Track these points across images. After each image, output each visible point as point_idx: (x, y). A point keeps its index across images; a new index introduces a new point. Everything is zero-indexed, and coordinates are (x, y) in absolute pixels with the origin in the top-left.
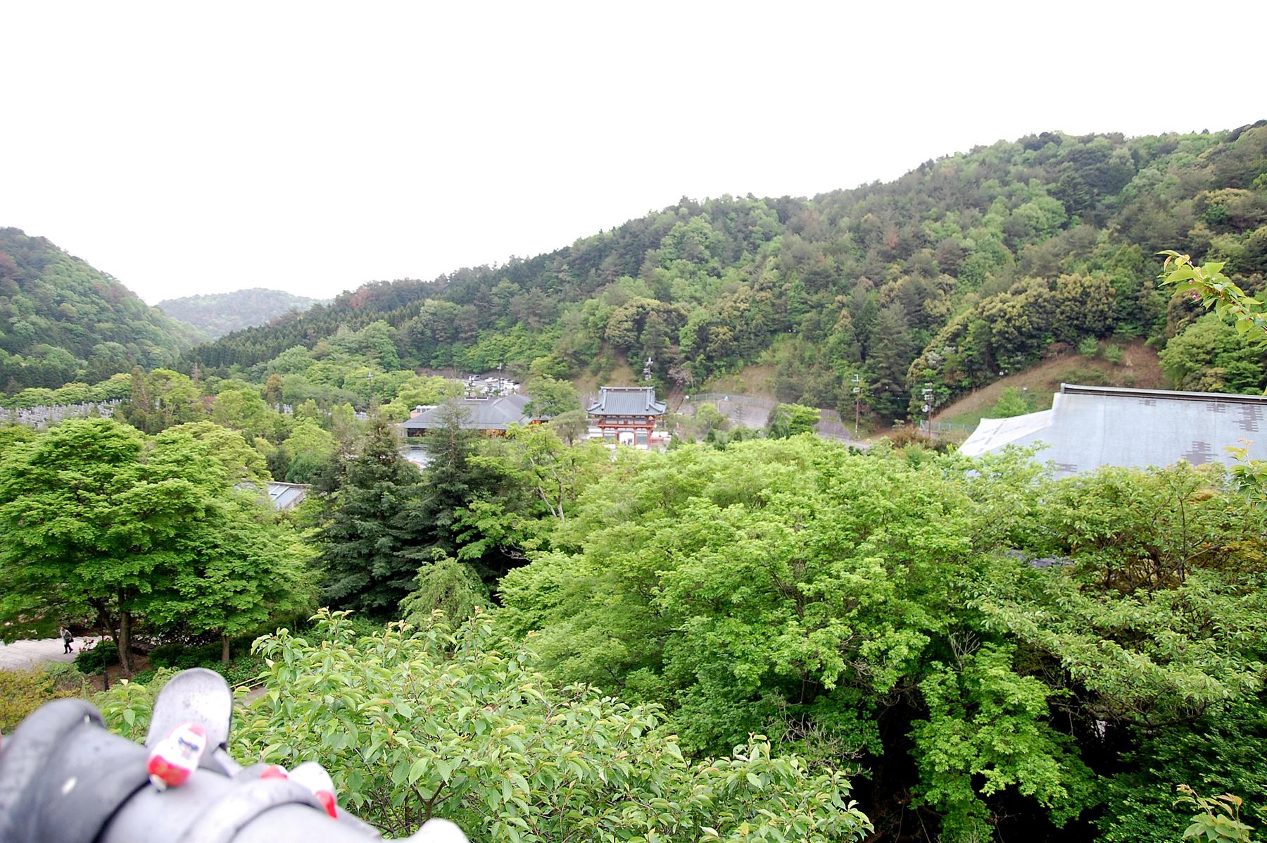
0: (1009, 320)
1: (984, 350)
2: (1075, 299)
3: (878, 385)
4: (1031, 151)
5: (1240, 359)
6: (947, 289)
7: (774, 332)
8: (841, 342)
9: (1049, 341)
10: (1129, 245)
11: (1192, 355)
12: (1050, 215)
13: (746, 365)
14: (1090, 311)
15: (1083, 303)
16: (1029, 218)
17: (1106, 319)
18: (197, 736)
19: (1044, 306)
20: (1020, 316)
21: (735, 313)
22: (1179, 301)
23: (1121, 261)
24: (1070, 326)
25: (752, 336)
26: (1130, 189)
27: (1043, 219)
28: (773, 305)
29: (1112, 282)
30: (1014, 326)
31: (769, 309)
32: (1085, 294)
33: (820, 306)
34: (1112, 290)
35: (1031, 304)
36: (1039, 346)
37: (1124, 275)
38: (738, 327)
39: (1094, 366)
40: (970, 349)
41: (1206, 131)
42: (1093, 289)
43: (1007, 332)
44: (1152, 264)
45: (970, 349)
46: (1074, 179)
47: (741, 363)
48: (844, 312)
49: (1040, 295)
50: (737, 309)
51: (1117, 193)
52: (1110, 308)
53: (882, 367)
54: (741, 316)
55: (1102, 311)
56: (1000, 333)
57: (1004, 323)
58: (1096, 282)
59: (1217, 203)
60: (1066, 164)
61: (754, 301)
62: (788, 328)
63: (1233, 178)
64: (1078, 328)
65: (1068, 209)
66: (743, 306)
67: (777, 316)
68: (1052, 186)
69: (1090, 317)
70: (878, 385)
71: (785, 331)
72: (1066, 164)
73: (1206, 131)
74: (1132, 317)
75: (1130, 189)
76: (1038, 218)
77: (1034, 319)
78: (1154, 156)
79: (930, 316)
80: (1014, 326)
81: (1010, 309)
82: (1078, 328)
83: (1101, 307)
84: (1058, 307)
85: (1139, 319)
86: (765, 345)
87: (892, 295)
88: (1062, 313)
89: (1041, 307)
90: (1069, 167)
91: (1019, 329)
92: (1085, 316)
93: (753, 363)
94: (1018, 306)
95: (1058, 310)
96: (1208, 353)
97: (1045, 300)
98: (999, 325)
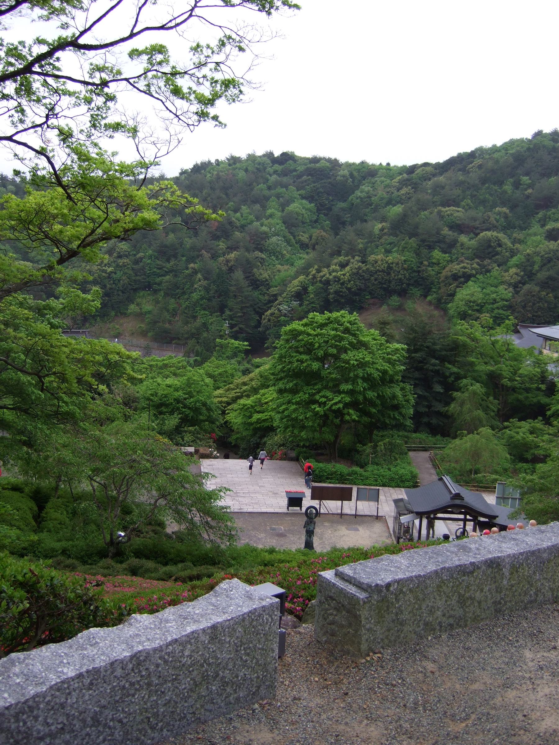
0: (343, 284)
1: (322, 303)
2: (383, 271)
3: (236, 329)
4: (277, 165)
5: (498, 308)
6: (262, 261)
7: (135, 290)
8: (202, 298)
9: (367, 297)
10: (410, 239)
11: (470, 307)
12: (309, 213)
13: (116, 315)
14: (393, 279)
15: (389, 274)
16: (297, 213)
17: (403, 284)
18: (289, 490)
19: (363, 276)
20: (350, 281)
21: (104, 274)
22: (450, 274)
23: (406, 248)
24: (381, 288)
25: (120, 293)
26: (354, 199)
27: (306, 215)
28: (133, 269)
29: (405, 261)
30: (346, 288)
31: (130, 272)
32: (390, 268)
33: (174, 272)
34: (405, 266)
35: (354, 274)
36: (360, 301)
37: (409, 256)
38: (108, 286)
39: (398, 314)
40: (313, 303)
41: (388, 164)
42: (394, 265)
43: (341, 292)
44: (425, 251)
45: (313, 303)
46: (318, 189)
47: (113, 313)
48: (199, 276)
49: (359, 268)
50: (105, 271)
51: (345, 201)
52: (405, 277)
53: (239, 316)
54: (109, 277)
55: (401, 279)
56: (336, 292)
57: (340, 286)
58: (396, 261)
59: (448, 215)
60: (305, 177)
61: (118, 266)
62: (148, 287)
63: (449, 200)
64: (385, 289)
65: (318, 210)
66: (110, 270)
67: (138, 278)
68: (302, 192)
69: (393, 283)
70: (236, 329)
71: (144, 289)
72: (305, 177)
73: (388, 164)
74: (417, 284)
75: (354, 199)
76: (303, 214)
77: (358, 283)
78: (364, 178)
79: (259, 280)
80: (346, 288)
81: (342, 276)
82: (385, 289)
83: (400, 276)
84: (371, 276)
85: (421, 285)
86: (131, 300)
87: (230, 265)
88: (376, 280)
89: (361, 276)
90: (309, 180)
91: (349, 289)
92: (390, 282)
93: (121, 314)
94: (348, 274)
95: (373, 278)
96: (477, 305)
97: (363, 271)
98: (332, 289)
